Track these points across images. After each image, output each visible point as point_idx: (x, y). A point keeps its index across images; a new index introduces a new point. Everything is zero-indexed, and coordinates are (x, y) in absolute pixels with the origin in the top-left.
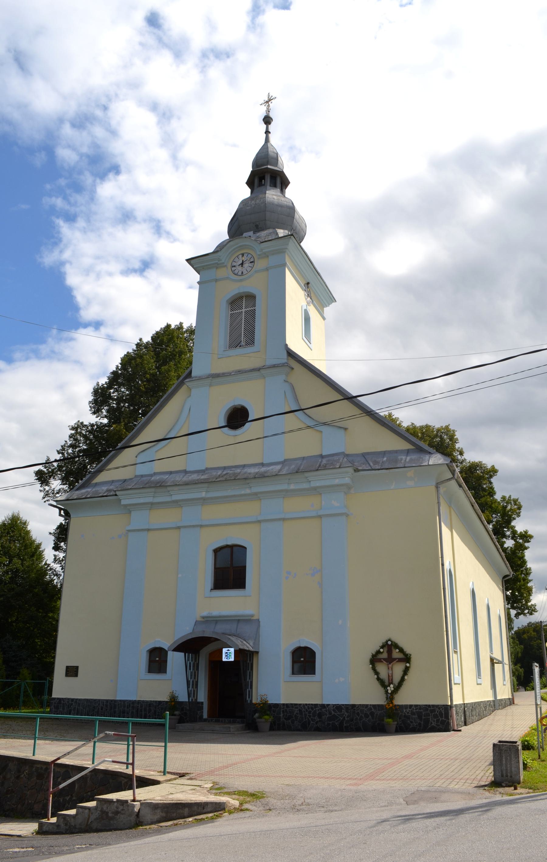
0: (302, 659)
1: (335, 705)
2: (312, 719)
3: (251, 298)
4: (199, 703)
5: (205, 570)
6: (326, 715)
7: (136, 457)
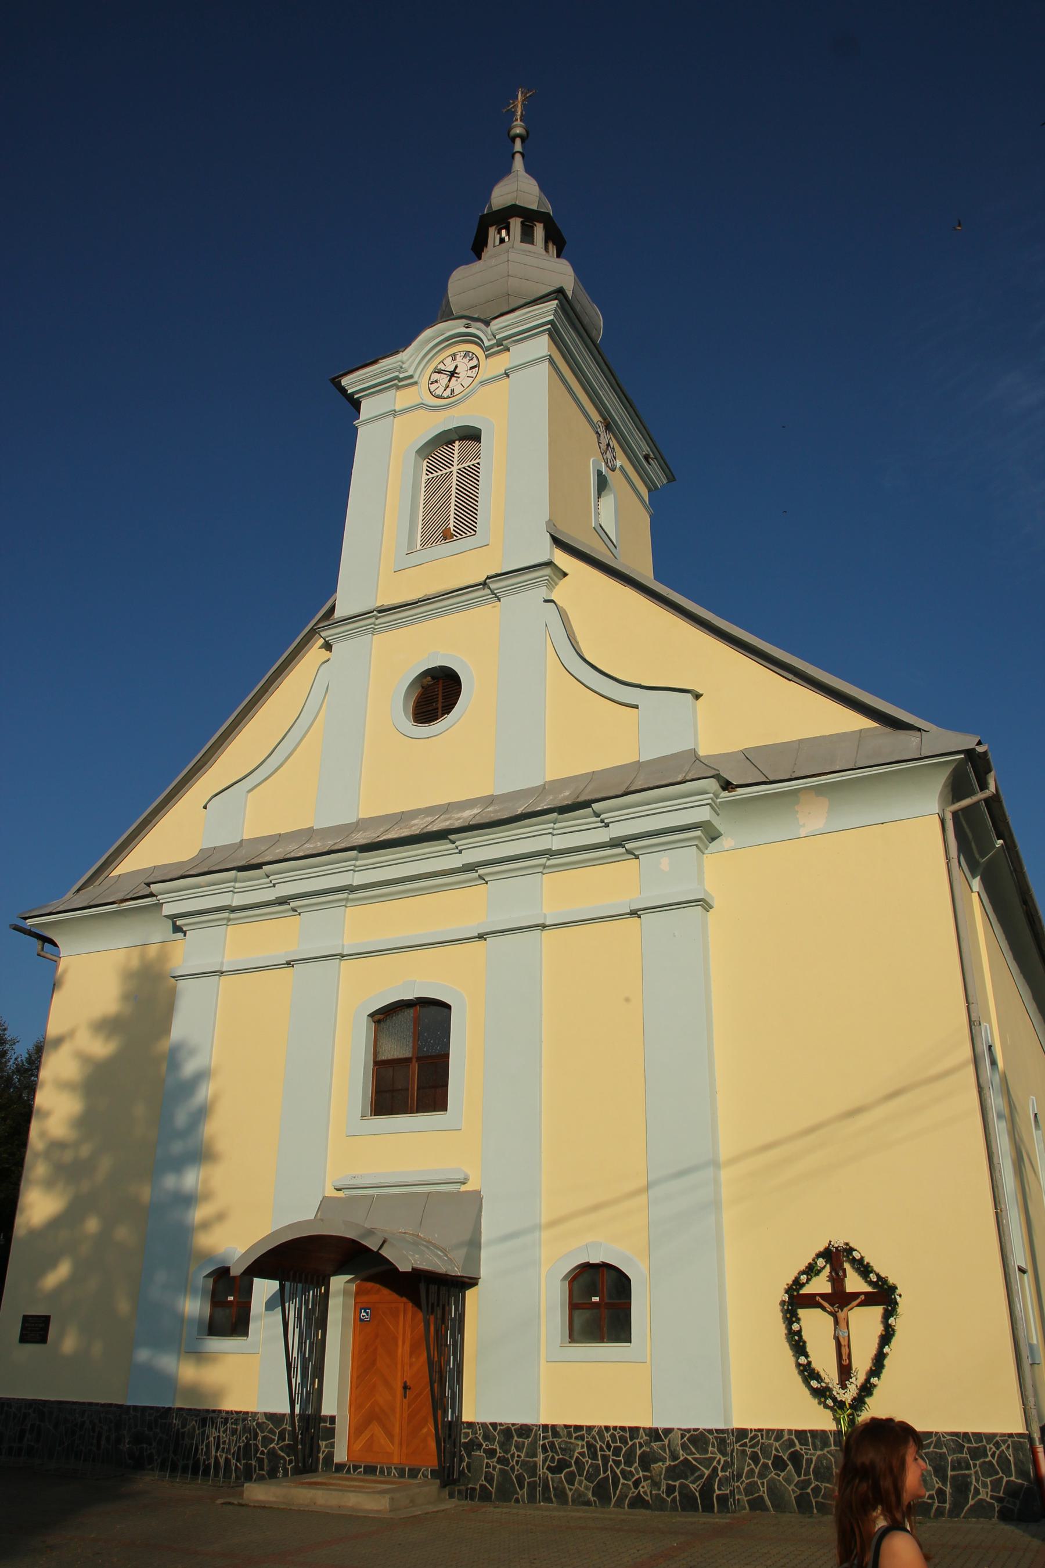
0: (596, 1299)
1: (688, 1430)
2: (623, 1472)
3: (471, 435)
4: (324, 1419)
5: (348, 1062)
6: (663, 1460)
7: (205, 807)
